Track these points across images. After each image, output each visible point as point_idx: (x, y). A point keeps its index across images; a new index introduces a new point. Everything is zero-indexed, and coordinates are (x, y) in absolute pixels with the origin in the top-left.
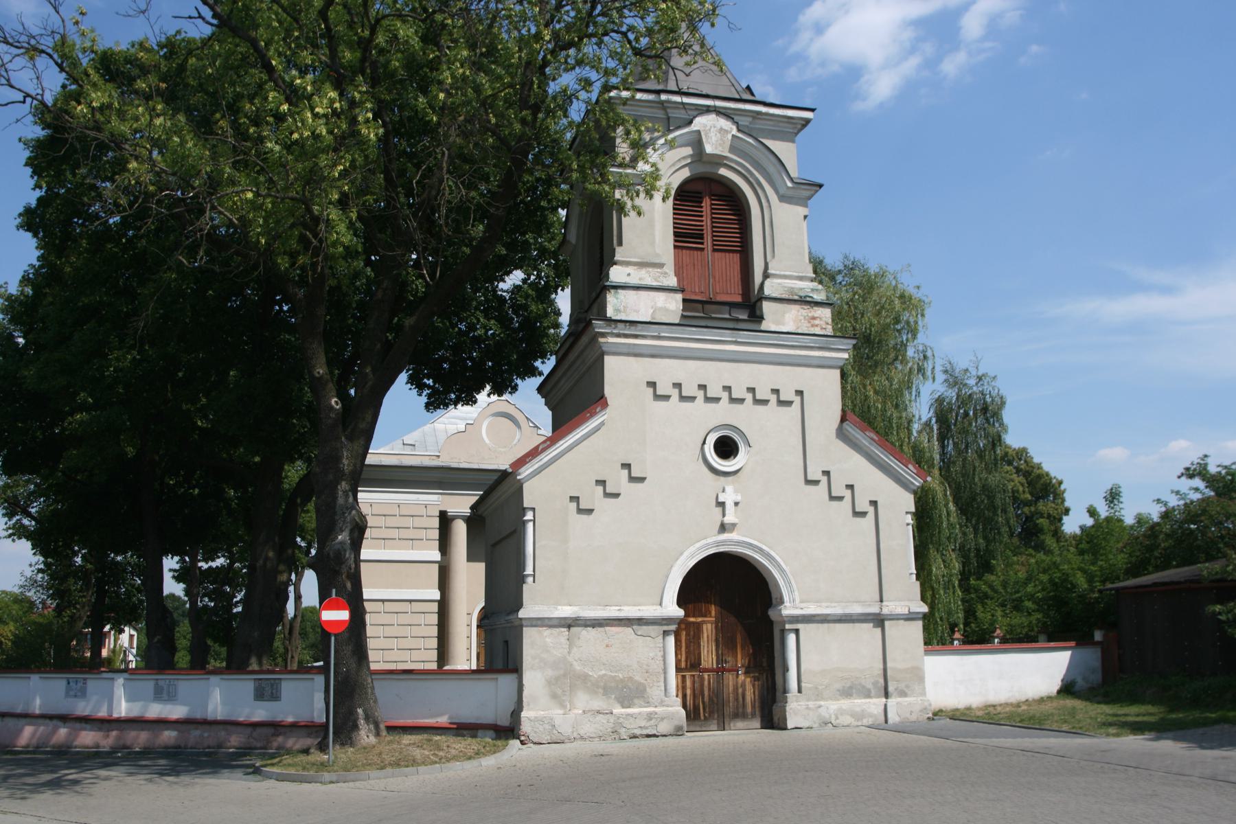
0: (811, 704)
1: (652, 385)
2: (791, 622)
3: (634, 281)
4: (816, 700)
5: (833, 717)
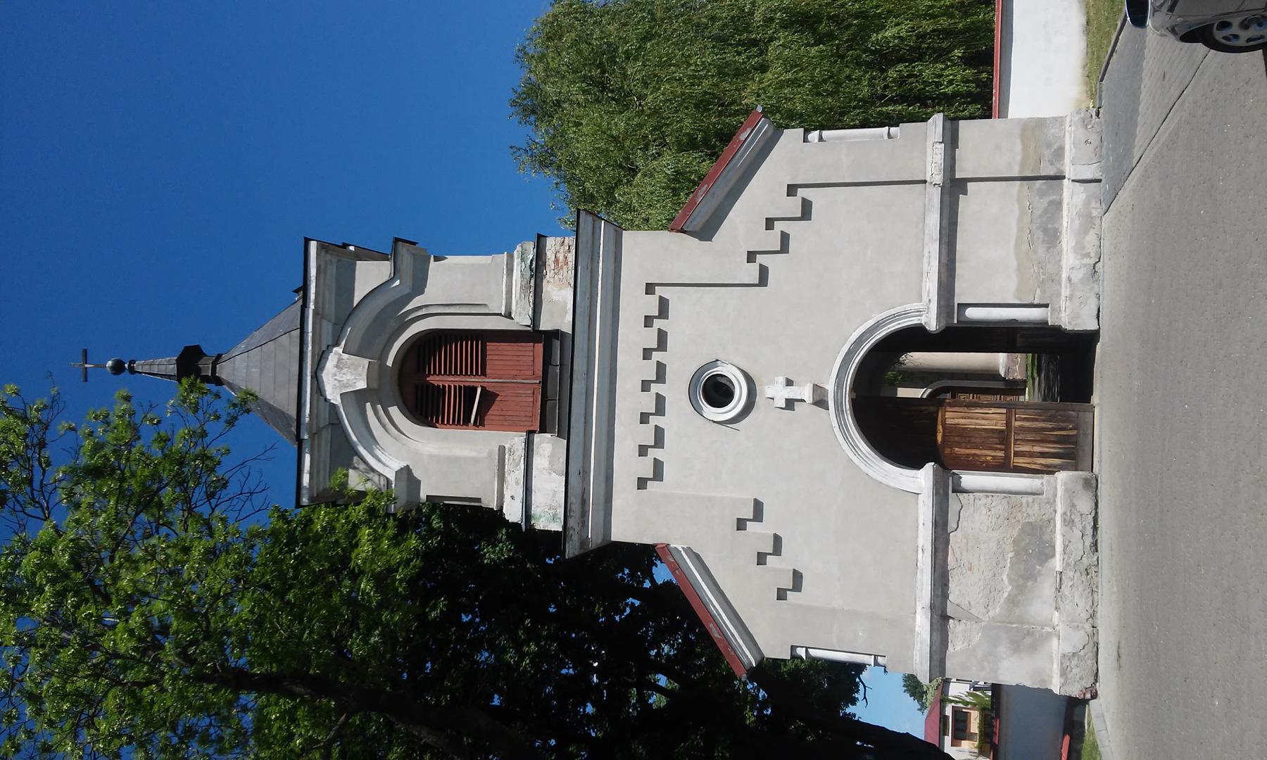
0: (1065, 292)
1: (642, 483)
2: (950, 315)
3: (519, 492)
4: (1060, 284)
5: (1086, 261)
